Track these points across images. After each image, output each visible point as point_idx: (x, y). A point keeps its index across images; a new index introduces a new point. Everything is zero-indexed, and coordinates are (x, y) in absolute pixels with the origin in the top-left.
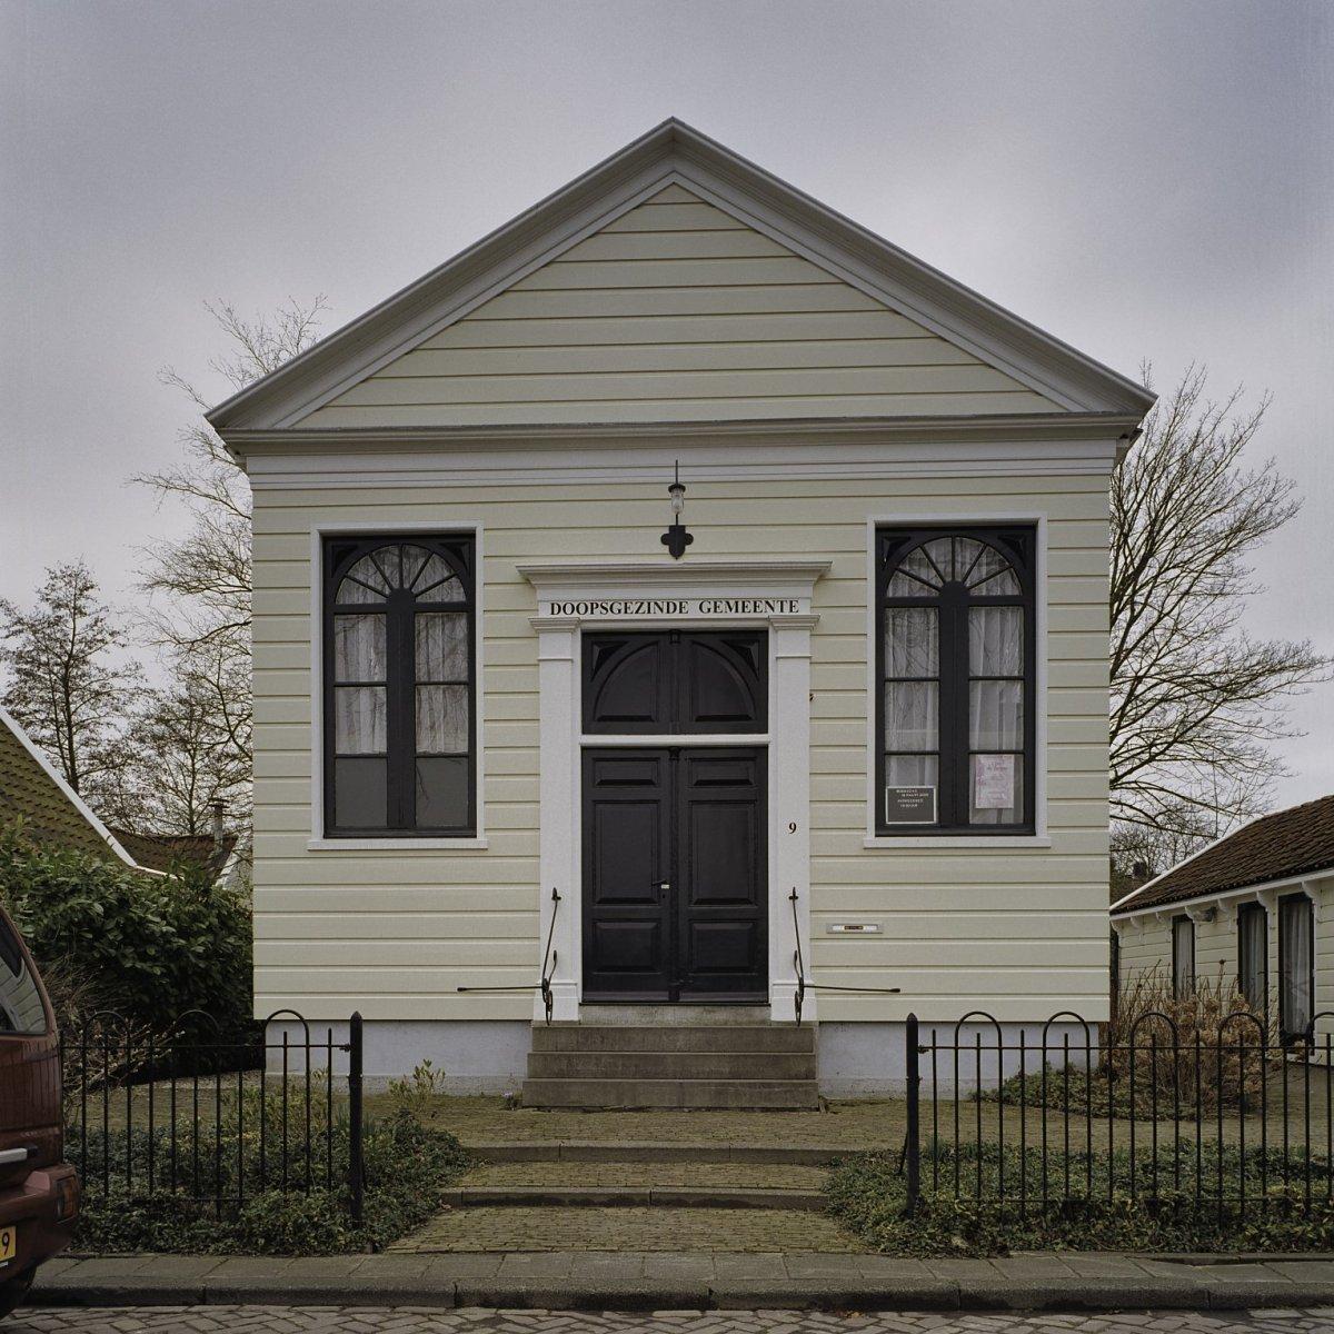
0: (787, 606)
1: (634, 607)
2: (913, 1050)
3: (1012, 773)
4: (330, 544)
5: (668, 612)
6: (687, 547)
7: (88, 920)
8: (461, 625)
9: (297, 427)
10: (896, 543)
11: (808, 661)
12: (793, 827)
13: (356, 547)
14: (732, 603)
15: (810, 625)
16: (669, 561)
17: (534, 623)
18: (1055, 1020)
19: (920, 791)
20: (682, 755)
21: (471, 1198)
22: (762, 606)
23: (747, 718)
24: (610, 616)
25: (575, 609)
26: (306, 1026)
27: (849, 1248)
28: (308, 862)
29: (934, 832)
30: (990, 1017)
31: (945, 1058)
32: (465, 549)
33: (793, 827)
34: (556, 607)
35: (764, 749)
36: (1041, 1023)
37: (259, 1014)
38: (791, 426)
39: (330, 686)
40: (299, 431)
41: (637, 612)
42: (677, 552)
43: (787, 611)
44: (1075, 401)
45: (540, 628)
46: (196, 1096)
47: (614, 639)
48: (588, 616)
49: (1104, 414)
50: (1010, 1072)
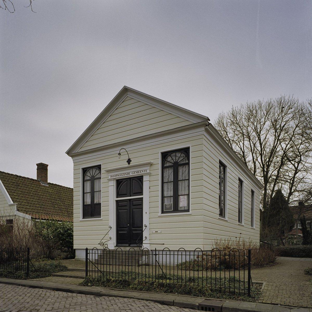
0: (145, 171)
1: (122, 175)
2: (87, 254)
3: (186, 199)
4: (163, 154)
7: (60, 233)
8: (187, 166)
9: (79, 151)
10: (165, 155)
11: (149, 181)
12: (146, 213)
13: (168, 154)
14: (137, 172)
15: (150, 174)
16: (128, 165)
17: (108, 180)
18: (94, 249)
19: (170, 204)
20: (131, 200)
21: (55, 275)
22: (142, 171)
23: (126, 194)
24: (119, 177)
28: (158, 218)
29: (173, 212)
30: (184, 249)
31: (161, 256)
32: (188, 151)
33: (146, 213)
35: (142, 198)
36: (162, 250)
37: (74, 248)
38: (142, 138)
39: (84, 193)
40: (76, 153)
42: (129, 164)
43: (145, 172)
44: (195, 121)
45: (110, 180)
46: (132, 262)
47: (121, 180)
48: (116, 177)
49: (202, 122)
50: (184, 261)
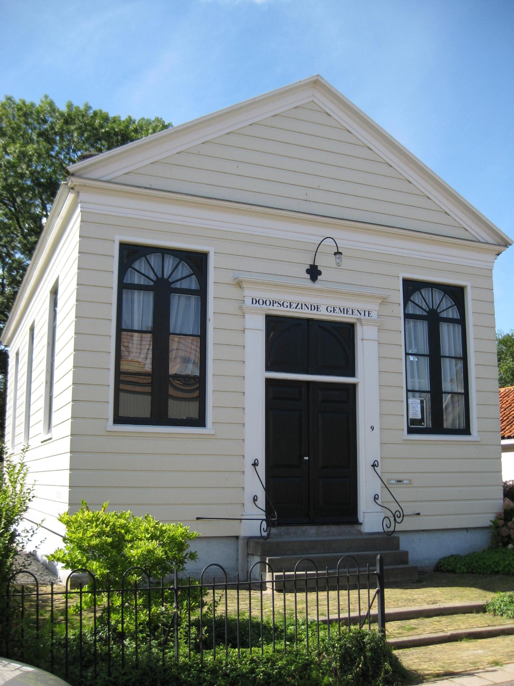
1: (294, 305)
5: (311, 310)
6: (319, 277)
12: (372, 428)
14: (342, 309)
25: (265, 302)
26: (389, 519)
27: (321, 643)
33: (372, 428)
34: (254, 300)
41: (296, 308)
